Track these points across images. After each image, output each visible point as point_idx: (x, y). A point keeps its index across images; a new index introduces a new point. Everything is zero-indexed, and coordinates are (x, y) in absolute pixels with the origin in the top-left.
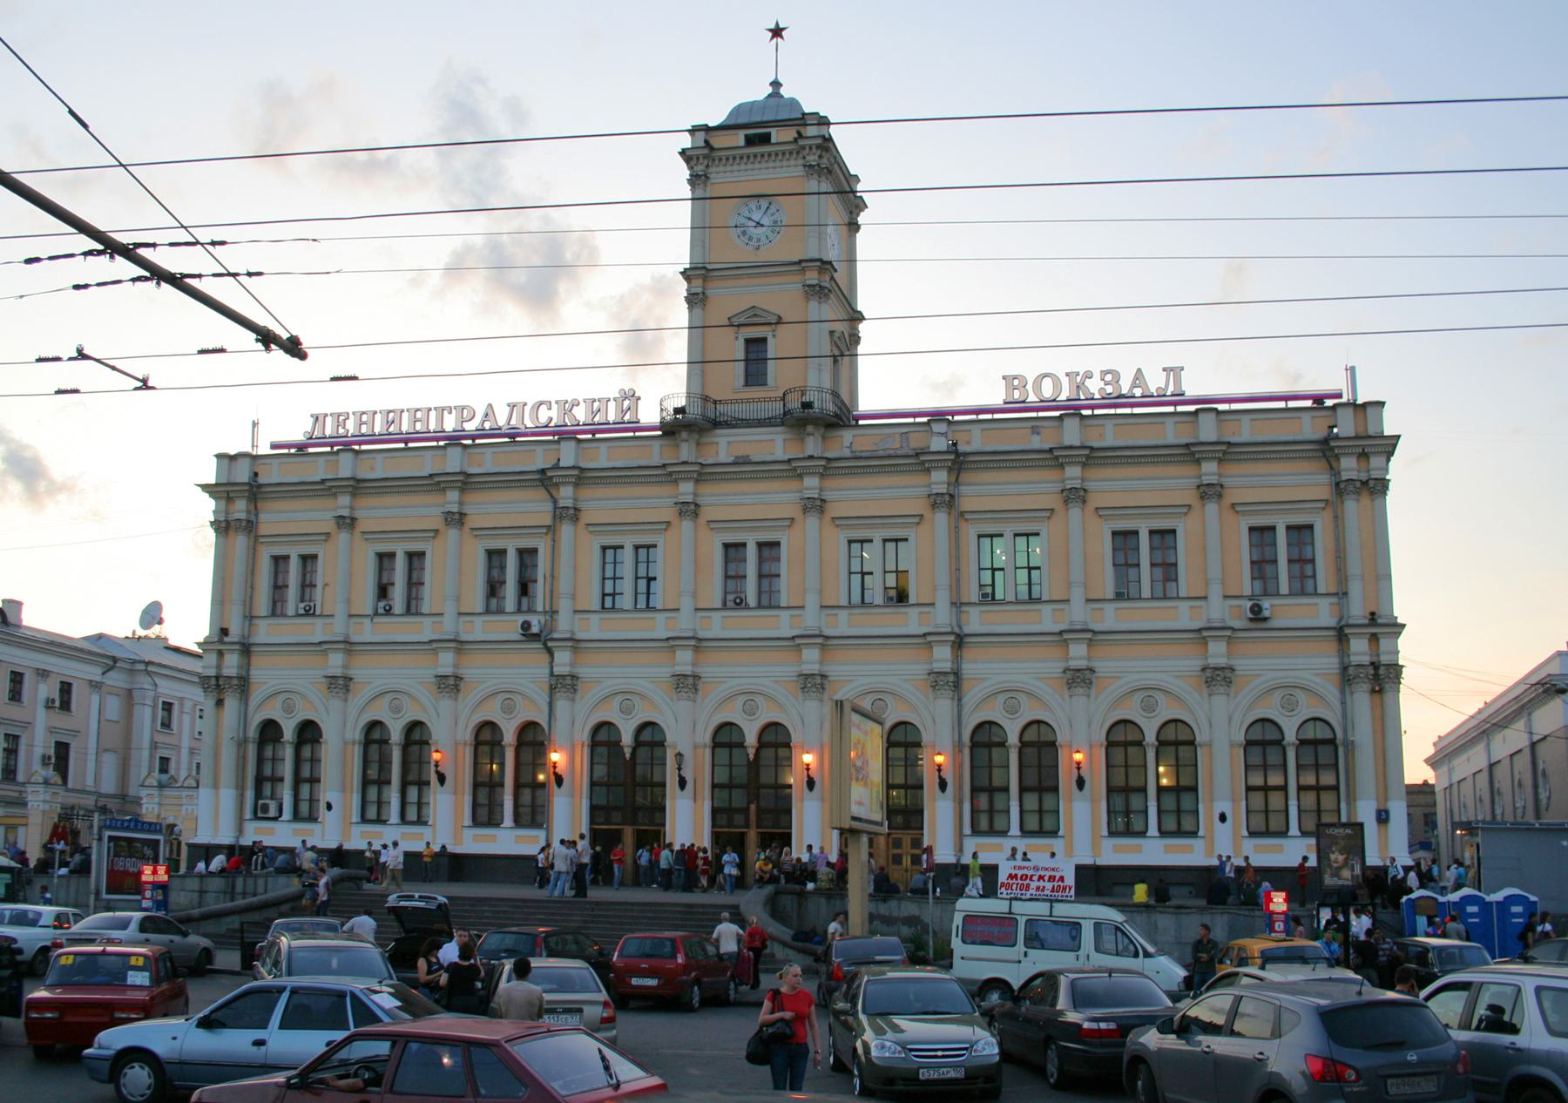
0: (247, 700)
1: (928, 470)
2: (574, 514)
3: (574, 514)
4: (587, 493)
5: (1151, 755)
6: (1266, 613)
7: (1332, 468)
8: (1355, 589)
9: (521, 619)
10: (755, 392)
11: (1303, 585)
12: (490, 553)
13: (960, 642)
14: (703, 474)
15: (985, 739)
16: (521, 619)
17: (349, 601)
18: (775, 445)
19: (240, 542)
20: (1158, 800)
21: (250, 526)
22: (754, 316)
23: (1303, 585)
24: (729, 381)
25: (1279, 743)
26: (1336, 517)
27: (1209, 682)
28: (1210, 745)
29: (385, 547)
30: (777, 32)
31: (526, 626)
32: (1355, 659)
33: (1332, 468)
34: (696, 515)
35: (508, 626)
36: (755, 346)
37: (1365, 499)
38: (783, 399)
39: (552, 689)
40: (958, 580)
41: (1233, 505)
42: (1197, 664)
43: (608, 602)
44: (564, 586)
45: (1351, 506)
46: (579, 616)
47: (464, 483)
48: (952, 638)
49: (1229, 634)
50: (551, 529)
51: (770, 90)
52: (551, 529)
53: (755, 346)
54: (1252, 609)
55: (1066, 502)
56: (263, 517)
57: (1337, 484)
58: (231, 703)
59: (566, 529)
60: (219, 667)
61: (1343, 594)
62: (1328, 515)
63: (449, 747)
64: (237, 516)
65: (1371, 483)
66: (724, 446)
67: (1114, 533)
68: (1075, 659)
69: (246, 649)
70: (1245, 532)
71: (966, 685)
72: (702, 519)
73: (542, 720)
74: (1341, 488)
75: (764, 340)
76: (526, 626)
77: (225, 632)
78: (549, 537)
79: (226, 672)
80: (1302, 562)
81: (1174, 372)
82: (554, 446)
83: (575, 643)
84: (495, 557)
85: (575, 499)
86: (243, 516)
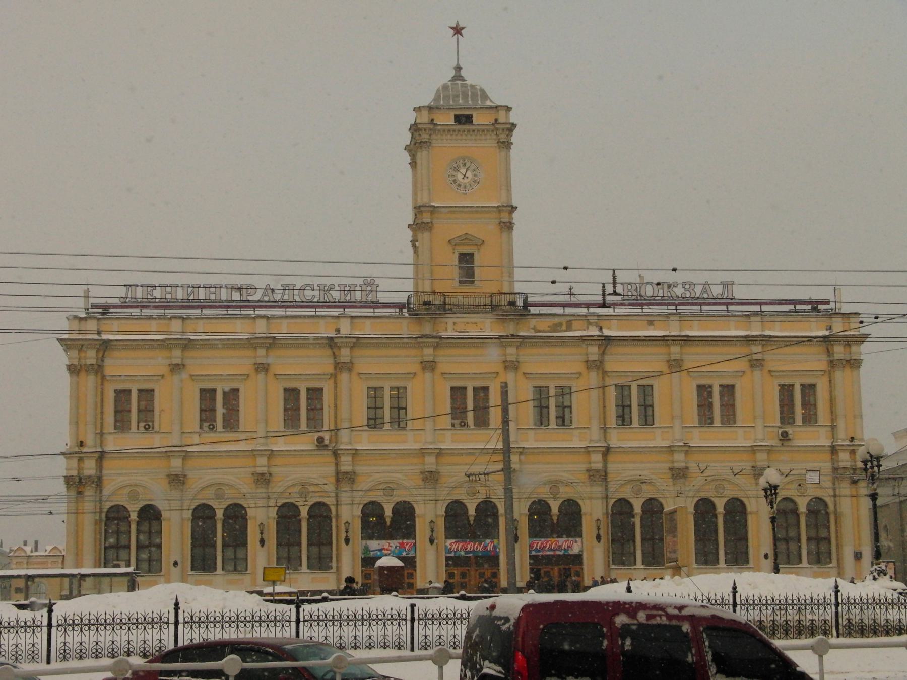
0: (101, 491)
1: (255, 348)
2: (349, 367)
3: (349, 367)
4: (358, 352)
5: (133, 527)
6: (790, 437)
7: (828, 351)
8: (841, 424)
9: (316, 435)
10: (466, 289)
11: (810, 418)
12: (700, 387)
13: (607, 451)
14: (439, 342)
15: (622, 509)
16: (316, 435)
17: (182, 424)
18: (488, 327)
19: (90, 382)
20: (223, 552)
21: (98, 369)
22: (466, 239)
23: (810, 418)
24: (448, 278)
25: (795, 512)
26: (830, 381)
27: (425, 480)
28: (756, 513)
29: (787, 381)
30: (458, 30)
31: (320, 440)
32: (842, 465)
33: (828, 351)
34: (516, 368)
35: (304, 443)
36: (466, 259)
37: (848, 371)
38: (491, 296)
39: (338, 480)
40: (832, 412)
41: (770, 371)
42: (584, 467)
43: (374, 422)
44: (344, 413)
45: (838, 374)
46: (438, 432)
47: (186, 345)
48: (603, 449)
49: (770, 450)
50: (334, 376)
51: (453, 73)
52: (334, 376)
53: (466, 259)
54: (318, 440)
55: (752, 366)
56: (108, 362)
57: (831, 361)
58: (89, 492)
59: (344, 377)
60: (80, 469)
61: (833, 427)
62: (825, 380)
63: (261, 516)
64: (89, 362)
65: (852, 362)
66: (450, 327)
67: (285, 390)
68: (594, 463)
69: (102, 456)
70: (282, 391)
71: (105, 482)
72: (438, 371)
73: (330, 501)
74: (339, 367)
75: (472, 255)
76: (320, 440)
77: (82, 444)
78: (332, 381)
79: (87, 473)
80: (809, 405)
81: (726, 285)
82: (335, 321)
83: (355, 453)
84: (291, 394)
85: (351, 357)
86: (94, 361)
